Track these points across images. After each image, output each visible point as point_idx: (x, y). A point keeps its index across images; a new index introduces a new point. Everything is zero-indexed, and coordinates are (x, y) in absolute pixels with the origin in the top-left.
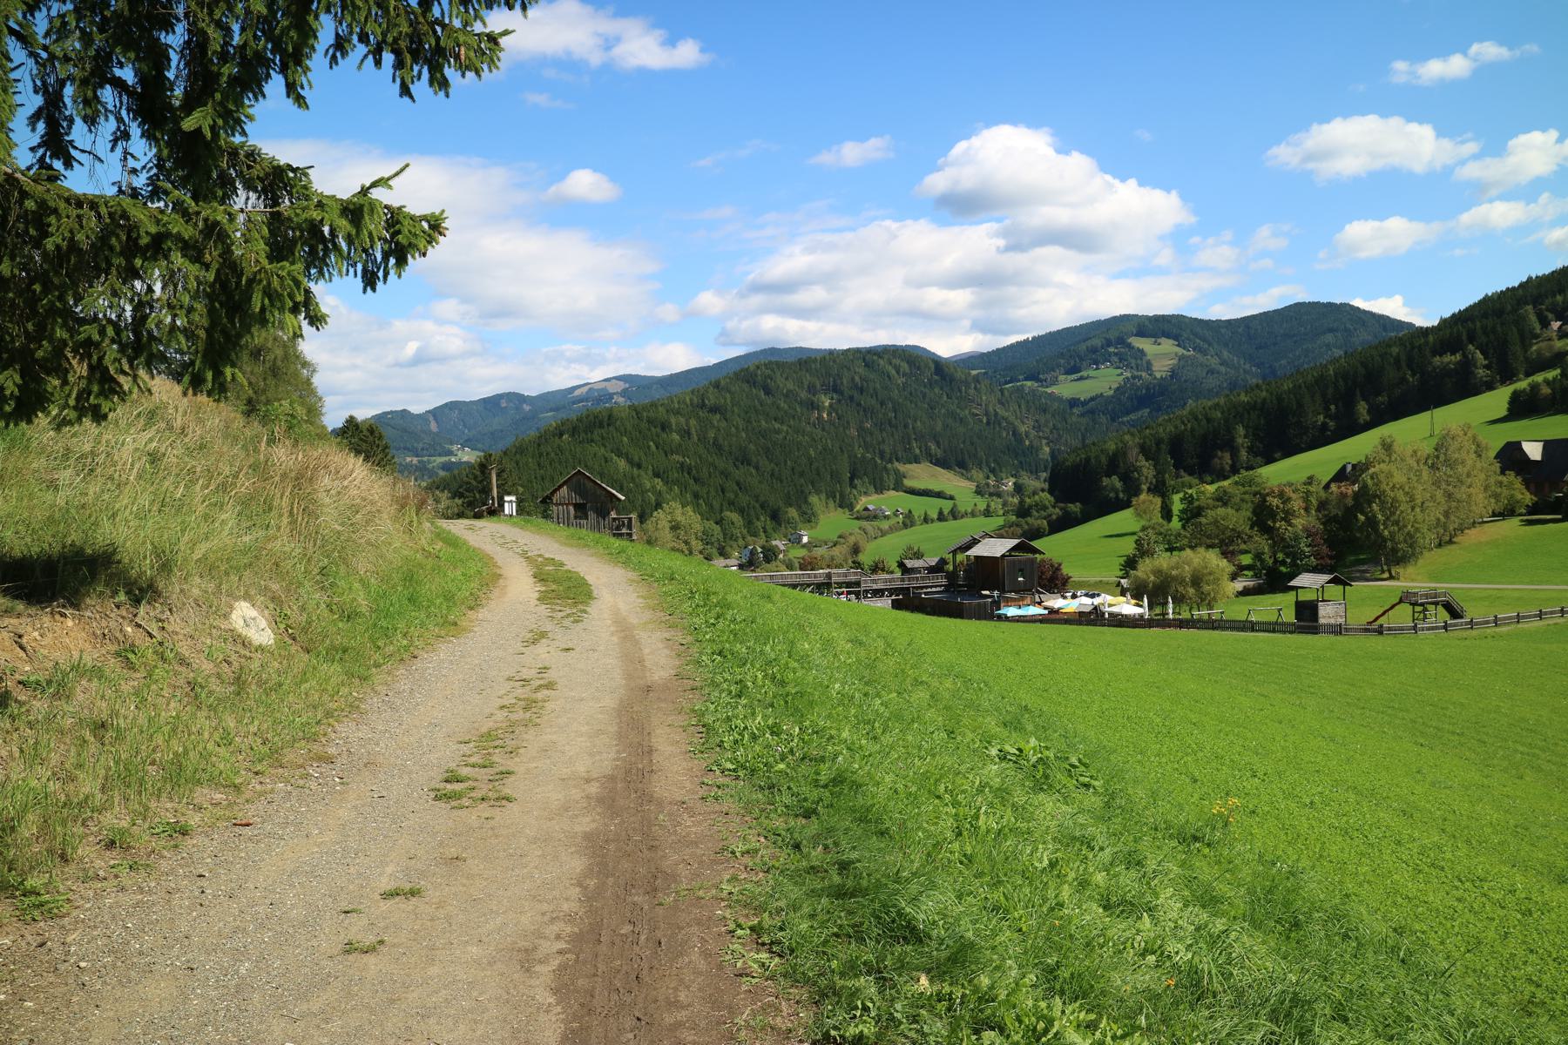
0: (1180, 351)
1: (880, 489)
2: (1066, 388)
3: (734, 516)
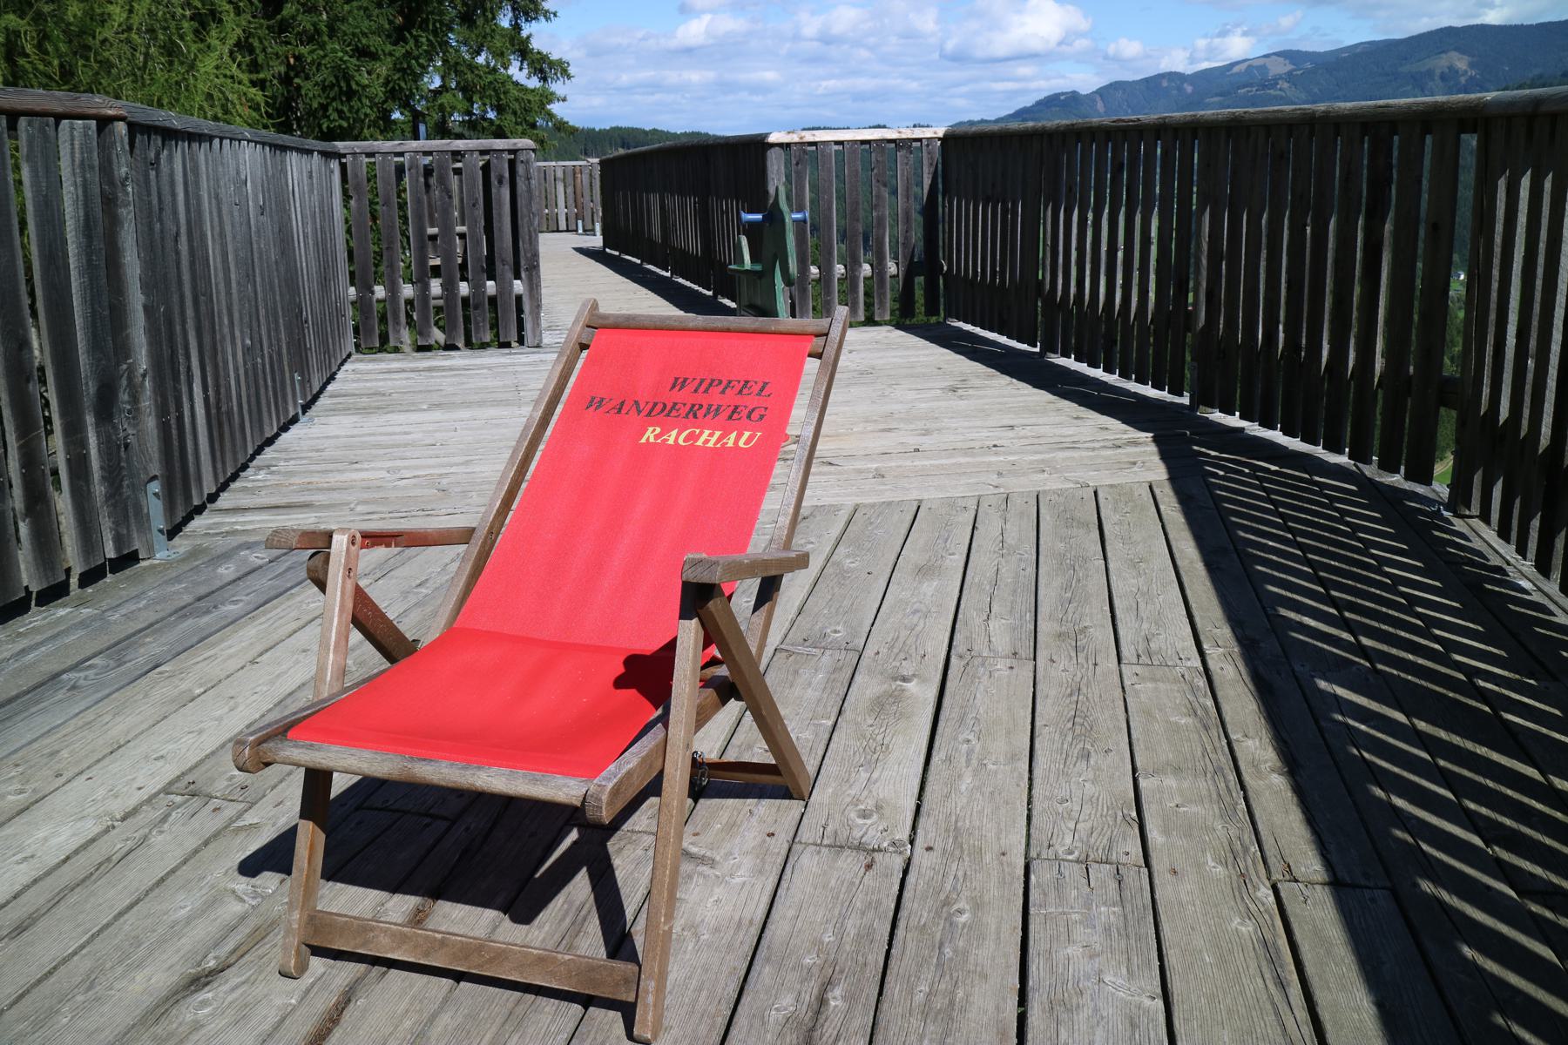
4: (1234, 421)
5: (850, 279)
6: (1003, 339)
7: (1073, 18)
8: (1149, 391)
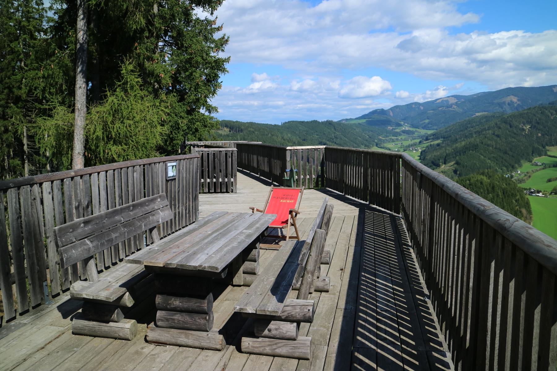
1: (540, 155)
3: (505, 168)
4: (375, 206)
5: (304, 179)
6: (337, 192)
7: (387, 85)
8: (362, 202)
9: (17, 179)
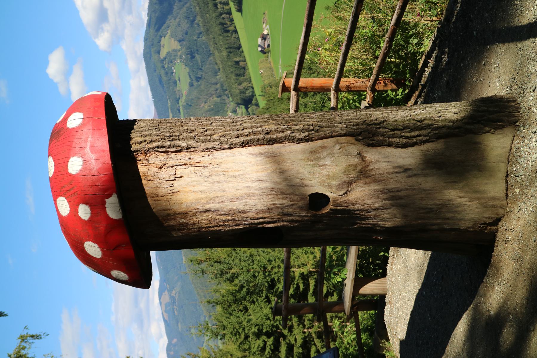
0: (168, 36)
2: (183, 86)
9: (376, 157)
